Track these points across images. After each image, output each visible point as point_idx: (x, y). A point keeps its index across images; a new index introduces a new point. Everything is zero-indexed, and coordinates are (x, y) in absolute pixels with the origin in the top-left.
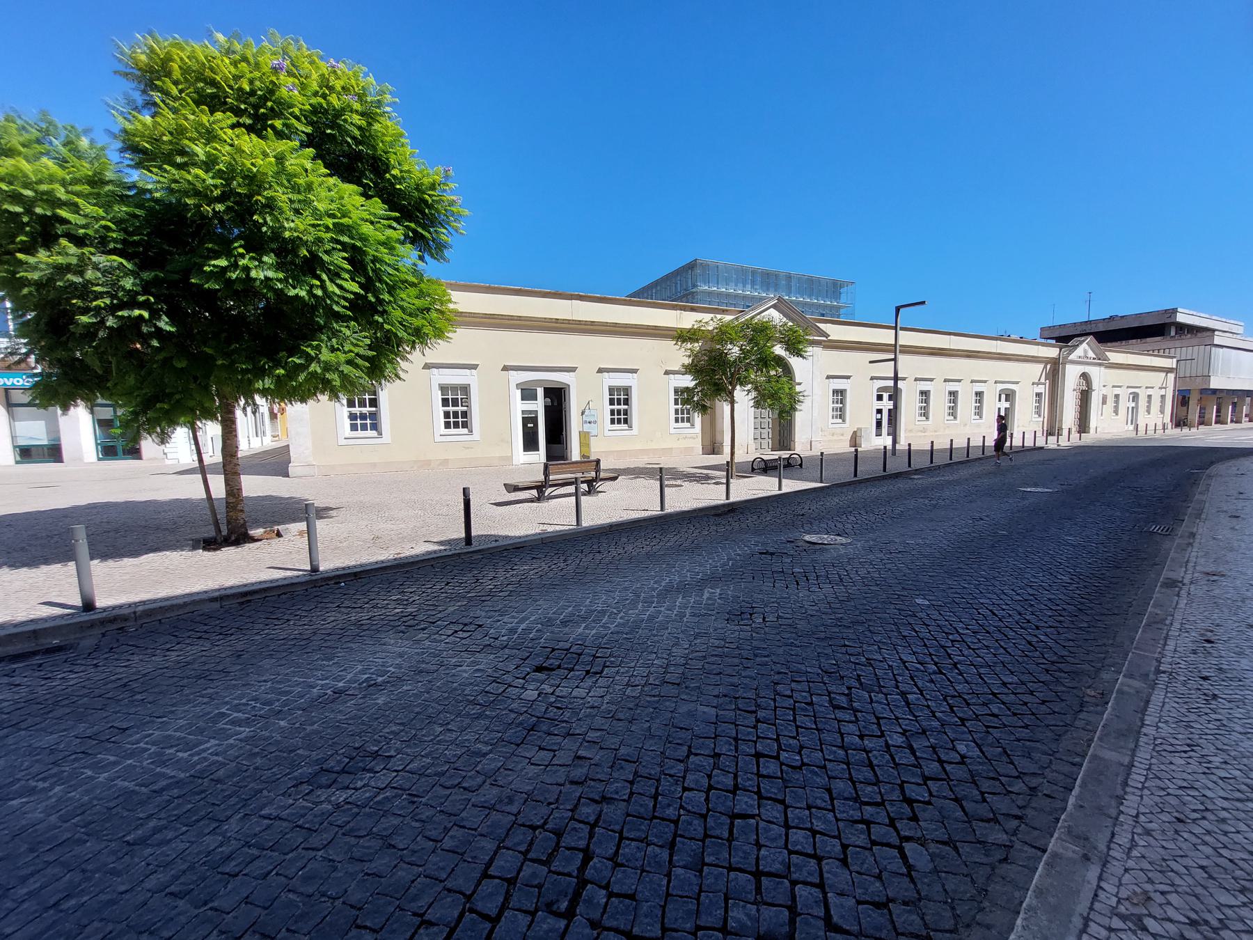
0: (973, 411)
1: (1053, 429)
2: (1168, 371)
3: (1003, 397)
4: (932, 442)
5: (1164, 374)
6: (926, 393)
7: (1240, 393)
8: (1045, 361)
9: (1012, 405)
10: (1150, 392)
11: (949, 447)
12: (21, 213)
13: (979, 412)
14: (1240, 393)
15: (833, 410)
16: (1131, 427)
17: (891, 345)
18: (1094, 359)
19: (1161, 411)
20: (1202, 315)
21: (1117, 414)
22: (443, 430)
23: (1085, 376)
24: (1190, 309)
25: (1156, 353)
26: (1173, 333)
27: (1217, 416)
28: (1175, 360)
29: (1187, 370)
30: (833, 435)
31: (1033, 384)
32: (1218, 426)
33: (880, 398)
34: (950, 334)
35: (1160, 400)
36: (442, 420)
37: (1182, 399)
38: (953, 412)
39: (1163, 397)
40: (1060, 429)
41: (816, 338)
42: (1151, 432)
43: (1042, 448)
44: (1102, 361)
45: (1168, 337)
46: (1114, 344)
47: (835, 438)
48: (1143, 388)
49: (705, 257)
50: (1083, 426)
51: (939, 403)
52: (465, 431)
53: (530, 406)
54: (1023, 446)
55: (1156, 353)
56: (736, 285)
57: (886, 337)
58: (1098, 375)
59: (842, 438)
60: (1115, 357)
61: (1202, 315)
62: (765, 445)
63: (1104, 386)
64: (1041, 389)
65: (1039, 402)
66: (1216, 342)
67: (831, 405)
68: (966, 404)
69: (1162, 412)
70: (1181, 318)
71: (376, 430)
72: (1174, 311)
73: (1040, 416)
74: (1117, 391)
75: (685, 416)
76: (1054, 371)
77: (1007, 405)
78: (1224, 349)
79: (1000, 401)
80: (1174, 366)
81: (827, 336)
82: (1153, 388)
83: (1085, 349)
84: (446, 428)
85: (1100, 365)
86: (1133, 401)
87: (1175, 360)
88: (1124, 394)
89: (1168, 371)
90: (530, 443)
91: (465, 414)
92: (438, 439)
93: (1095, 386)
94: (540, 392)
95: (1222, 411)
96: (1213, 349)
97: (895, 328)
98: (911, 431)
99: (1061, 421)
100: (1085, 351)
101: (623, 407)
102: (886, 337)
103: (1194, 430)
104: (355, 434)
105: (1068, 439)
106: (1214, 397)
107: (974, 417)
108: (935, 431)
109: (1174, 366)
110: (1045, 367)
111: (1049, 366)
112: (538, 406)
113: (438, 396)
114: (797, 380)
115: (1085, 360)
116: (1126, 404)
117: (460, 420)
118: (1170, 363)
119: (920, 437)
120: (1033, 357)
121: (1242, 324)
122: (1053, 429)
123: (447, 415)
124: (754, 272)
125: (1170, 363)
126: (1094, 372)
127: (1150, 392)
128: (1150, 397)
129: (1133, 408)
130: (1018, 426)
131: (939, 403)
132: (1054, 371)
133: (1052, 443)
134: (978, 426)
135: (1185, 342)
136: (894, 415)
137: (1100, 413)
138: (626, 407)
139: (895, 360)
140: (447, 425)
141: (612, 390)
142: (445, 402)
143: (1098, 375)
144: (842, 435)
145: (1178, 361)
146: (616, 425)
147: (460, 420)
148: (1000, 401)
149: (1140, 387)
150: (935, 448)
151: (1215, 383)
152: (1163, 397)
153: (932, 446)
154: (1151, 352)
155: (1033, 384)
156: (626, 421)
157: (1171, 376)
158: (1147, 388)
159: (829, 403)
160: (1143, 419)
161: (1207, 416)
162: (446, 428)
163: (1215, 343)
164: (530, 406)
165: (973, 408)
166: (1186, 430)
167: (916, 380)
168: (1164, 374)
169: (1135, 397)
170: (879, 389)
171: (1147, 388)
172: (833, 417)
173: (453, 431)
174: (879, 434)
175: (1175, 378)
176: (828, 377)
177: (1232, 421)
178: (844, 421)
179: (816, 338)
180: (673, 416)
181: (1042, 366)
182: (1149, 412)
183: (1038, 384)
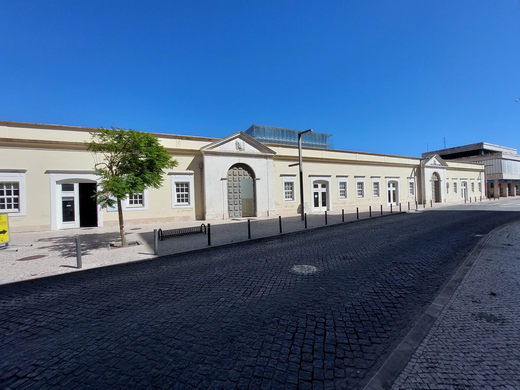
0: (409, 191)
1: (421, 201)
2: (481, 171)
3: (391, 185)
4: (343, 210)
5: (479, 173)
6: (361, 183)
7: (519, 181)
8: (414, 166)
9: (397, 189)
10: (472, 181)
11: (369, 211)
12: (426, 163)
13: (456, 191)
14: (519, 181)
15: (340, 192)
16: (300, 215)
17: (297, 157)
18: (439, 165)
20: (496, 146)
21: (474, 192)
23: (435, 174)
24: (490, 143)
25: (478, 163)
26: (483, 153)
27: (509, 192)
28: (484, 166)
29: (491, 170)
30: (286, 207)
31: (408, 178)
32: (510, 197)
33: (316, 186)
35: (478, 185)
36: (176, 198)
37: (490, 185)
38: (344, 193)
39: (480, 184)
40: (425, 201)
41: (267, 154)
42: (478, 201)
43: (405, 213)
44: (444, 167)
45: (480, 155)
46: (455, 159)
47: (288, 208)
48: (469, 179)
49: (256, 124)
50: (438, 199)
51: (352, 188)
52: (187, 203)
53: (68, 194)
54: (392, 212)
55: (478, 163)
56: (287, 138)
57: (294, 152)
58: (442, 173)
59: (292, 208)
60: (451, 164)
61: (496, 146)
62: (237, 213)
63: (447, 179)
64: (412, 180)
65: (412, 187)
67: (373, 189)
68: (368, 188)
69: (480, 190)
70: (486, 147)
71: (142, 203)
72: (482, 144)
73: (413, 194)
74: (455, 181)
76: (419, 172)
77: (394, 189)
78: (508, 160)
80: (484, 169)
81: (275, 153)
83: (433, 161)
84: (178, 202)
85: (443, 168)
86: (464, 186)
87: (484, 166)
88: (459, 183)
89: (481, 171)
90: (68, 216)
93: (442, 178)
94: (76, 186)
95: (511, 190)
96: (502, 160)
97: (299, 148)
98: (336, 204)
99: (425, 196)
100: (435, 162)
101: (185, 193)
102: (294, 152)
103: (497, 200)
104: (132, 205)
105: (430, 205)
106: (506, 184)
107: (410, 194)
108: (351, 203)
109: (484, 169)
110: (414, 170)
111: (416, 169)
112: (75, 194)
113: (175, 187)
114: (257, 177)
115: (435, 166)
116: (460, 187)
117: (185, 198)
118: (482, 167)
119: (342, 206)
120: (406, 164)
121: (516, 150)
122: (421, 201)
123: (178, 196)
124: (282, 131)
125: (482, 167)
126: (440, 171)
127: (472, 181)
128: (473, 183)
129: (465, 189)
131: (352, 188)
132: (419, 172)
133: (421, 208)
134: (377, 200)
135: (488, 158)
136: (395, 193)
137: (446, 192)
138: (187, 193)
139: (299, 164)
140: (179, 201)
142: (178, 190)
143: (442, 173)
144: (293, 207)
145: (485, 166)
146: (288, 199)
147: (185, 198)
149: (467, 179)
150: (359, 212)
151: (505, 177)
152: (480, 184)
153: (343, 212)
154: (475, 163)
155: (408, 178)
156: (141, 202)
157: (483, 174)
158: (471, 179)
159: (372, 188)
160: (470, 194)
161: (504, 193)
162: (178, 202)
163: (503, 157)
164: (316, 190)
165: (409, 190)
166: (492, 200)
168: (479, 173)
169: (465, 184)
170: (314, 182)
171: (471, 179)
172: (340, 195)
173: (181, 203)
175: (485, 174)
176: (281, 176)
177: (517, 195)
178: (378, 196)
179: (267, 154)
181: (412, 169)
182: (473, 190)
183: (410, 178)
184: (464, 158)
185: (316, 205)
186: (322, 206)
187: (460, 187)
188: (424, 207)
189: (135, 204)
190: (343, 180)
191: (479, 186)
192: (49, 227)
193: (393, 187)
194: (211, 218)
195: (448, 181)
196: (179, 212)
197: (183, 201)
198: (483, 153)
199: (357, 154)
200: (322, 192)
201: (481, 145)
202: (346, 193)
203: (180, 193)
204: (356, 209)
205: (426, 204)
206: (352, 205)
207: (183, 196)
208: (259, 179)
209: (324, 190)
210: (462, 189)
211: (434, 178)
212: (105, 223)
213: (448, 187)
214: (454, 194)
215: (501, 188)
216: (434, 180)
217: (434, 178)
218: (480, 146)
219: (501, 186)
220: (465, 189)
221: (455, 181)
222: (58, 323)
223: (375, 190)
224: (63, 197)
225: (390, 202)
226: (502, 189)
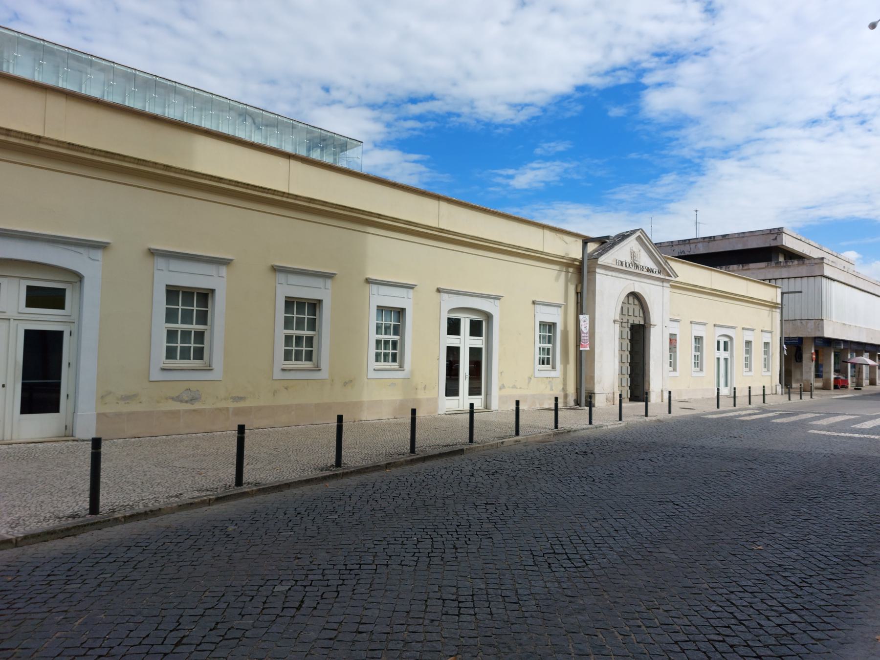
2: (773, 306)
13: (698, 363)
18: (649, 270)
19: (765, 367)
22: (280, 361)
29: (798, 309)
32: (837, 391)
33: (454, 327)
34: (438, 198)
42: (757, 401)
45: (773, 264)
64: (553, 316)
66: (826, 273)
75: (391, 351)
78: (836, 282)
79: (718, 349)
82: (753, 330)
84: (168, 357)
85: (663, 280)
86: (725, 349)
87: (779, 291)
91: (310, 340)
92: (156, 375)
93: (655, 317)
100: (633, 255)
104: (172, 363)
115: (633, 269)
123: (171, 335)
125: (772, 294)
126: (652, 292)
130: (502, 387)
140: (171, 353)
141: (289, 303)
142: (171, 316)
145: (782, 294)
148: (718, 349)
149: (734, 328)
154: (767, 282)
157: (777, 314)
164: (453, 341)
167: (743, 329)
174: (452, 390)
180: (280, 347)
182: (673, 365)
184: (735, 267)
185: (452, 390)
186: (23, 411)
187: (710, 353)
191: (766, 353)
193: (471, 335)
195: (674, 329)
197: (185, 354)
198: (781, 259)
199: (444, 205)
200: (27, 332)
201: (777, 233)
203: (179, 326)
204: (235, 433)
205: (594, 407)
206: (241, 404)
207: (186, 334)
209: (478, 342)
210: (718, 359)
211: (631, 313)
213: (748, 351)
214: (745, 374)
215: (820, 362)
216: (631, 321)
217: (631, 313)
218: (776, 239)
219: (820, 358)
220: (726, 359)
221: (699, 331)
223: (544, 349)
225: (52, 406)
226: (822, 366)
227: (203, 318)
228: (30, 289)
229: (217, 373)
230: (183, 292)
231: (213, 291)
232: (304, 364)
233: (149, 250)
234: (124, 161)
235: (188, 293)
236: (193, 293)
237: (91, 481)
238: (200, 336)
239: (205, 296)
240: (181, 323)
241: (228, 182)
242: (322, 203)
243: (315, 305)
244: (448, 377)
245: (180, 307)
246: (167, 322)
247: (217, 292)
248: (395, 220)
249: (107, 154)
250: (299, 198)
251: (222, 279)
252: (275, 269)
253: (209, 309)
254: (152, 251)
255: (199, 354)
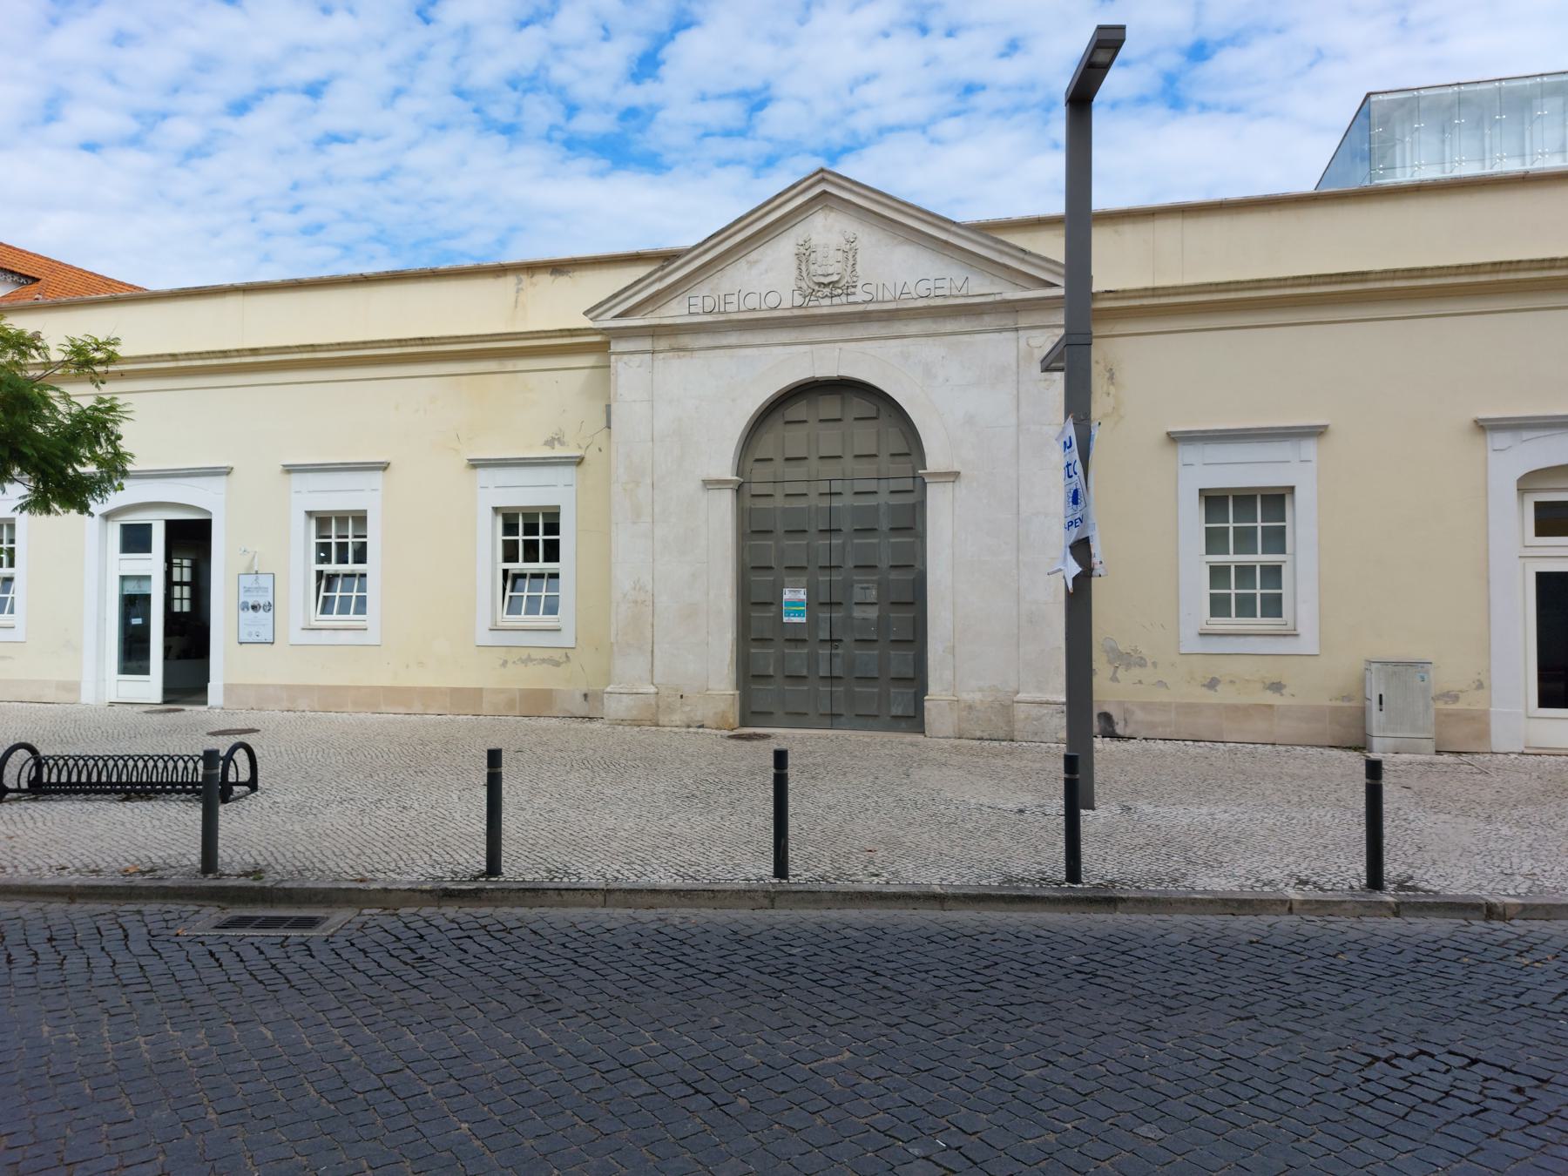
30: (1212, 684)
36: (1204, 591)
53: (137, 564)
59: (1271, 698)
90: (133, 653)
104: (1221, 624)
113: (1194, 520)
140: (1219, 606)
142: (1215, 541)
144: (1277, 687)
173: (1233, 623)
188: (781, 758)
189: (1237, 615)
190: (337, 496)
192: (74, 687)
194: (634, 714)
196: (505, 663)
202: (1286, 591)
203: (1232, 558)
207: (1245, 572)
208: (710, 484)
212: (229, 689)
222: (1381, 1140)
224: (123, 578)
227: (1276, 540)
228: (1539, 506)
229: (1308, 642)
230: (353, 517)
231: (1292, 489)
232: (1259, 623)
233: (1168, 434)
234: (1477, 273)
235: (1244, 499)
236: (1256, 496)
237: (1382, 825)
238: (1273, 574)
239: (1276, 500)
240: (1263, 553)
241: (1527, 266)
242: (1538, 265)
243: (1207, 498)
244: (176, 640)
245: (1231, 525)
246: (1208, 552)
247: (1297, 491)
248: (536, 335)
249: (1497, 266)
250: (1429, 273)
251: (1309, 464)
252: (1482, 427)
253: (1288, 524)
254: (1481, 424)
255: (1273, 606)
